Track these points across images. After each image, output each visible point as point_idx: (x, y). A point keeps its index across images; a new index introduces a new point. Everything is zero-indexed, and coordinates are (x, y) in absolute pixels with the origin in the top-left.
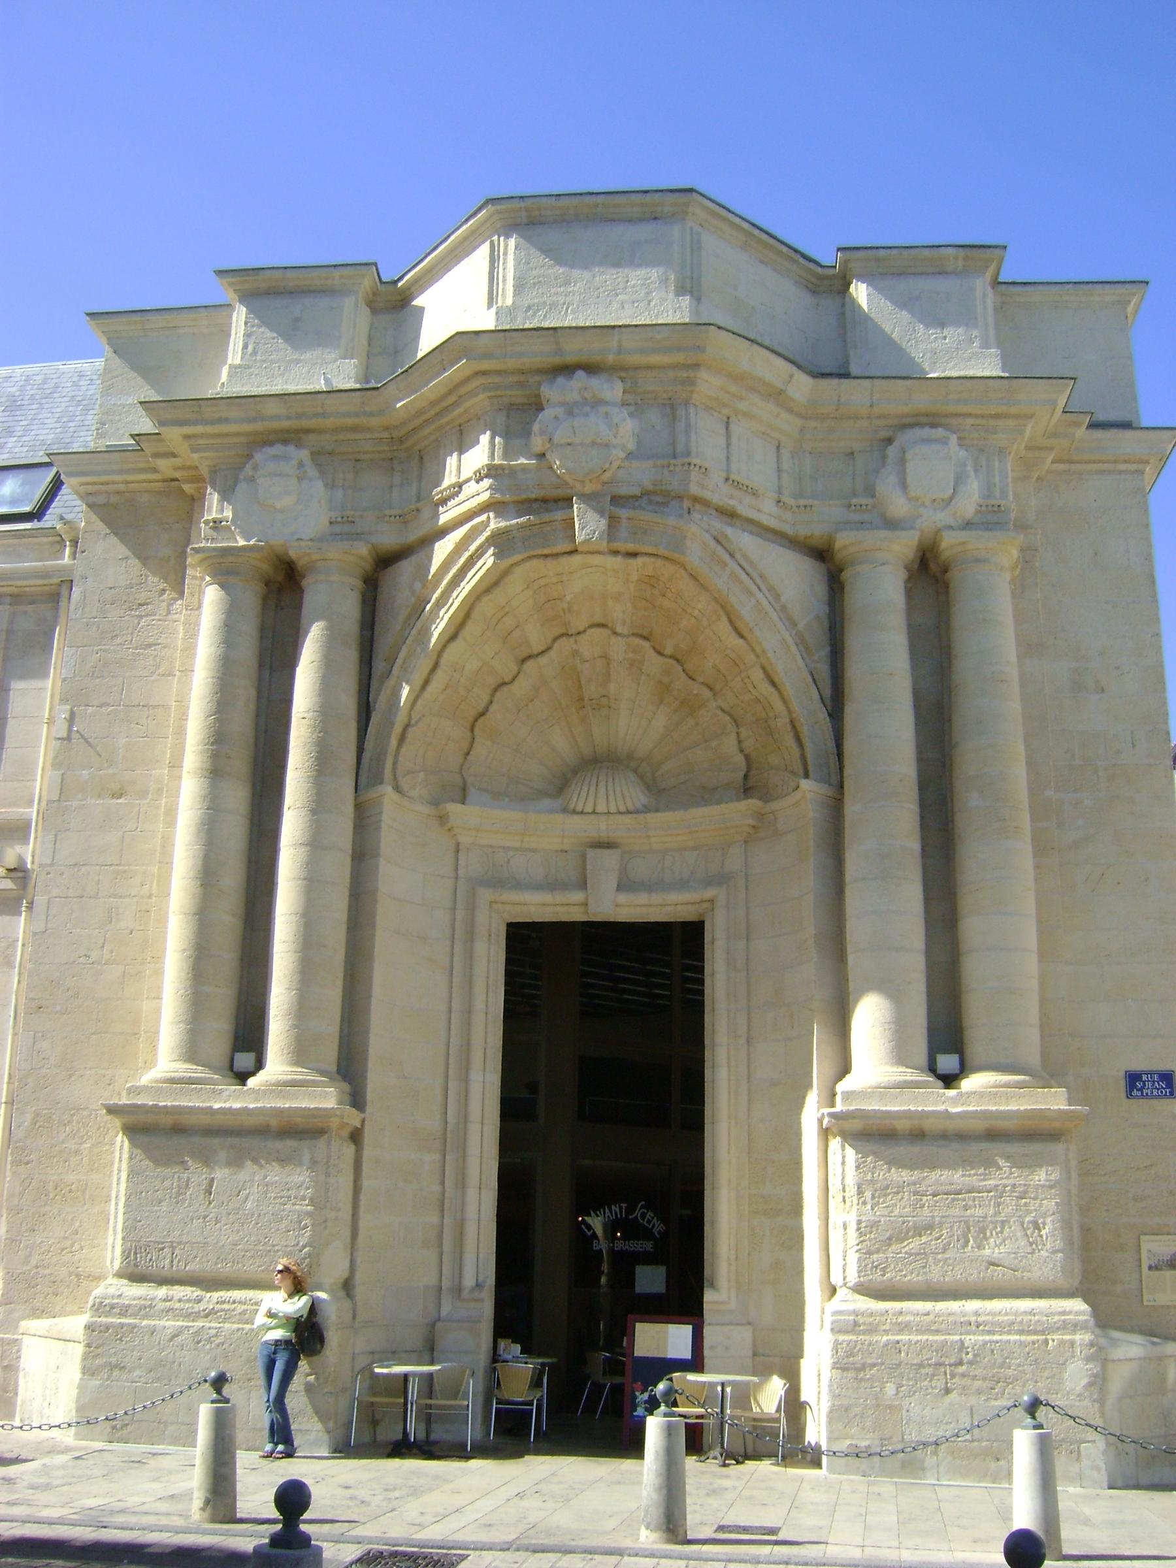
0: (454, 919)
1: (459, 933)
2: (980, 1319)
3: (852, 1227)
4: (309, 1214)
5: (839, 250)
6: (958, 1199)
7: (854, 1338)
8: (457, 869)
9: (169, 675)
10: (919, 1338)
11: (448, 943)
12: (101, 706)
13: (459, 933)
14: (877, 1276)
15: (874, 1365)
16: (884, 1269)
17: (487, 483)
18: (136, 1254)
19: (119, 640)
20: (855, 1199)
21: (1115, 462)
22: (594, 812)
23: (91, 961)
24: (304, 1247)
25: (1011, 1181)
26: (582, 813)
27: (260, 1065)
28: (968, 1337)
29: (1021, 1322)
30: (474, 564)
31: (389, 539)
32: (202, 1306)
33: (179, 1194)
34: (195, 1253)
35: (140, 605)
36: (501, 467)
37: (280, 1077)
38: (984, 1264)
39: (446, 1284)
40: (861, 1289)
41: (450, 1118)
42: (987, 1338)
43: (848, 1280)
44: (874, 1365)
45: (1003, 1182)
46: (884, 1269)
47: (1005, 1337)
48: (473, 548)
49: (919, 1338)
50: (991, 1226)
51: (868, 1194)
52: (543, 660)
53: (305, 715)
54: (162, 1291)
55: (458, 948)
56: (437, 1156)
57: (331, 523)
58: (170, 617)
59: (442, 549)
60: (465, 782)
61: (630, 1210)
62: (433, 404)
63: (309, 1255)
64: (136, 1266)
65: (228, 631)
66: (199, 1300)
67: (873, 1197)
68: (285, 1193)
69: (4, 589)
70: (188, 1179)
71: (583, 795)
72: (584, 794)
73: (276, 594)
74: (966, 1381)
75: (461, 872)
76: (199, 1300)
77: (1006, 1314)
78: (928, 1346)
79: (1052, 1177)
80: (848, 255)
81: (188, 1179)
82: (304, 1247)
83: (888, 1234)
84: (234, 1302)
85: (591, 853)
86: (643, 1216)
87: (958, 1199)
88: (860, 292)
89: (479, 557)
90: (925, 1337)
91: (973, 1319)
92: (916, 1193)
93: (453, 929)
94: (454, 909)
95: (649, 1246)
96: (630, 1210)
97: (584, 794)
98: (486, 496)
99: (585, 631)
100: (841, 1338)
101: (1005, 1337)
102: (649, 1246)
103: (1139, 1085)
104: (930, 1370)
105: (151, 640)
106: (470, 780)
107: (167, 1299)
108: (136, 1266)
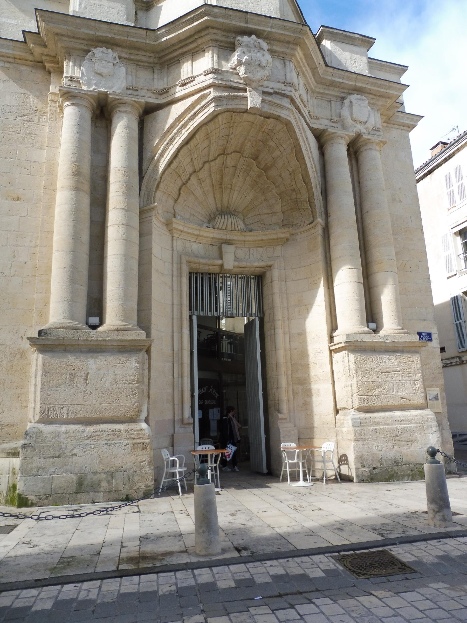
0: (173, 267)
1: (175, 273)
2: (402, 419)
3: (355, 386)
4: (137, 388)
5: (322, 26)
6: (389, 374)
7: (361, 428)
8: (173, 247)
9: (41, 149)
10: (383, 427)
11: (171, 277)
12: (5, 158)
13: (175, 273)
14: (364, 404)
15: (368, 438)
16: (367, 401)
17: (211, 76)
18: (48, 411)
19: (13, 130)
20: (355, 375)
21: (401, 125)
22: (226, 229)
23: (4, 275)
24: (135, 403)
25: (406, 368)
26: (221, 229)
27: (101, 322)
28: (398, 426)
29: (414, 419)
30: (202, 111)
31: (154, 100)
32: (85, 434)
33: (70, 381)
34: (80, 409)
35: (24, 115)
36: (216, 69)
37: (118, 326)
38: (400, 398)
39: (176, 418)
40: (360, 409)
41: (175, 349)
42: (405, 426)
43: (354, 406)
44: (368, 438)
45: (404, 368)
46: (367, 401)
47: (410, 425)
48: (203, 103)
49: (383, 427)
50: (401, 384)
51: (359, 373)
52: (213, 164)
53: (120, 169)
54: (64, 428)
55: (175, 279)
56: (170, 364)
57: (127, 89)
58: (39, 123)
59: (176, 110)
60: (175, 213)
61: (209, 389)
62: (181, 41)
63: (137, 407)
64: (48, 417)
65: (80, 127)
66: (83, 431)
67: (361, 374)
68: (124, 379)
69: (3, 50)
70: (75, 374)
71: (220, 221)
72: (222, 221)
73: (102, 113)
74: (400, 442)
75: (175, 248)
76: (83, 431)
77: (409, 416)
78: (386, 430)
79: (418, 366)
80: (325, 29)
81: (75, 374)
82: (135, 403)
83: (368, 388)
84: (102, 431)
85: (223, 246)
86: (213, 391)
87: (389, 374)
88: (327, 44)
89: (207, 106)
90: (385, 427)
91: (399, 419)
92: (376, 372)
93: (173, 271)
94: (173, 263)
95: (214, 402)
96: (209, 389)
97: (222, 221)
98: (211, 81)
99: (231, 153)
100: (357, 429)
101: (410, 425)
102: (214, 402)
103: (422, 337)
104: (387, 439)
105: (31, 132)
106: (177, 211)
107: (66, 432)
108: (48, 417)
